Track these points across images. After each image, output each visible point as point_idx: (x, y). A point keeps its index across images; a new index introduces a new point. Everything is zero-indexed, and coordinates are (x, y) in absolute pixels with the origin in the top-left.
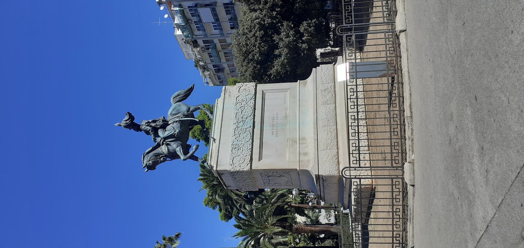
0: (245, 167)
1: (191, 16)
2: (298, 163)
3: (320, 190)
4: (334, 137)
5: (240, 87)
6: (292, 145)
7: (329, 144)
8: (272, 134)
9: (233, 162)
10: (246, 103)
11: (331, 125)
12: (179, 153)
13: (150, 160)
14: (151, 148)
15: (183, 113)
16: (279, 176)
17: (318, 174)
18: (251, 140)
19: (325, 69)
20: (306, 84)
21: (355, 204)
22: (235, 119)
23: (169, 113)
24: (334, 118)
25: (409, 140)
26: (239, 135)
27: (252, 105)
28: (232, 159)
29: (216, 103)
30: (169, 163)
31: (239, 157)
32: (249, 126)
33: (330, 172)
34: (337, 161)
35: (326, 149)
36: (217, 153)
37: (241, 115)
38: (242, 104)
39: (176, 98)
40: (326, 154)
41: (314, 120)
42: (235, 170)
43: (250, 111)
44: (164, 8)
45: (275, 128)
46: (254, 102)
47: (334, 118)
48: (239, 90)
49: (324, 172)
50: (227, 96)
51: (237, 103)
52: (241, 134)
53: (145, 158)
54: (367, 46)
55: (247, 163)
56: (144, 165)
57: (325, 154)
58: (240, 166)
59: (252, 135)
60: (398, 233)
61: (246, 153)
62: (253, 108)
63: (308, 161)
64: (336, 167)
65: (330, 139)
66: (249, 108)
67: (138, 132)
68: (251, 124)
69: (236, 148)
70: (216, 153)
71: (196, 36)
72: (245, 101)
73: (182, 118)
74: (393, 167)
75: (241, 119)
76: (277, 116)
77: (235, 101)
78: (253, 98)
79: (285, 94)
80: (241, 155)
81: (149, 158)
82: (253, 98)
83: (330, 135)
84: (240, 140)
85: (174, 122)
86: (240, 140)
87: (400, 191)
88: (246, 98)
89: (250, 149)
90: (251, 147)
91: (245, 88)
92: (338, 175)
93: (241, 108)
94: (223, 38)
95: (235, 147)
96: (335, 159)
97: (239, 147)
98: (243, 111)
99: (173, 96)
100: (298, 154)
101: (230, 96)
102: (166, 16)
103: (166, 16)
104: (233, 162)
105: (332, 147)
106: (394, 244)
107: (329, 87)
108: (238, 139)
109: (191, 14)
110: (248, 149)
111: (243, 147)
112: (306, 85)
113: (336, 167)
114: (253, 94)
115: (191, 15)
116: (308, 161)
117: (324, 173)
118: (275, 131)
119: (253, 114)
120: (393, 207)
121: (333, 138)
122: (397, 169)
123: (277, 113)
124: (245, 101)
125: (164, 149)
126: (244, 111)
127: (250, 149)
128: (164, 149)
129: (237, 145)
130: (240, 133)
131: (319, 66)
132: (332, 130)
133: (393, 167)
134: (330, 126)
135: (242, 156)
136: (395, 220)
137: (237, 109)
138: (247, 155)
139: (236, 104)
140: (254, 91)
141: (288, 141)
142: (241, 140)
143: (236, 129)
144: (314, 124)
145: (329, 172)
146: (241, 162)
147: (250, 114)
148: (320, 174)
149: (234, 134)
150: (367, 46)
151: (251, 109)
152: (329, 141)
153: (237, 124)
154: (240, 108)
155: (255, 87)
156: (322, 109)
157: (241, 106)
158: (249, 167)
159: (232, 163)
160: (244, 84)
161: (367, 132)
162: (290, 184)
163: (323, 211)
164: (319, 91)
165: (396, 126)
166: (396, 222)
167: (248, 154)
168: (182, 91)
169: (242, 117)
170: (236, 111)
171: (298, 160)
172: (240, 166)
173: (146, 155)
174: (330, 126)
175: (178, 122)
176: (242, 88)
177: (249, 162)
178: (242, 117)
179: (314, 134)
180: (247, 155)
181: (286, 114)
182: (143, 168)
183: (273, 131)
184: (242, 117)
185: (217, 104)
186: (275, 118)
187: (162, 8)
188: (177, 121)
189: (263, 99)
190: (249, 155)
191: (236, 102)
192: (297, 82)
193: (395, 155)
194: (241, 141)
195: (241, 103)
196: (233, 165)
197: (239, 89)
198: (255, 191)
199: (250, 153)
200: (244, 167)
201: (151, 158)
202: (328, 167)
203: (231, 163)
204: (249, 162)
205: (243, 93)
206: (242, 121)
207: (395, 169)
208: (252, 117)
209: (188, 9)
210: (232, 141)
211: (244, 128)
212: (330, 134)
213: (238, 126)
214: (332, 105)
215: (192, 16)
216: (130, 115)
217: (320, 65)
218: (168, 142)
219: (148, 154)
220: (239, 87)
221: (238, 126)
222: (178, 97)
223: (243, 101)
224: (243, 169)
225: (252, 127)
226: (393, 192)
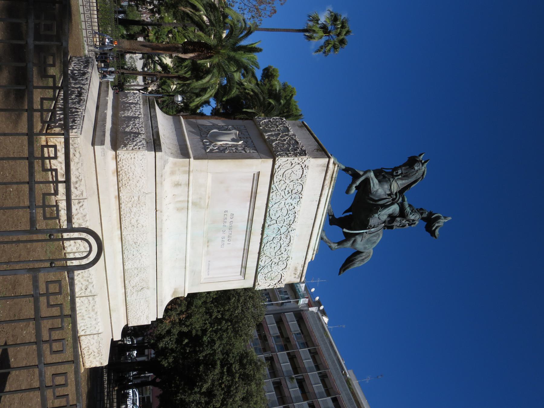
0: (284, 163)
2: (191, 169)
4: (126, 217)
5: (279, 282)
6: (200, 198)
7: (134, 205)
8: (233, 214)
9: (303, 171)
10: (272, 261)
11: (131, 235)
12: (376, 181)
13: (417, 171)
14: (412, 187)
15: (363, 238)
17: (156, 153)
18: (270, 205)
19: (142, 320)
20: (175, 292)
21: (57, 130)
22: (292, 237)
23: (381, 237)
24: (125, 247)
26: (288, 213)
27: (263, 258)
28: (303, 176)
29: (314, 255)
30: (388, 165)
31: (291, 180)
32: (271, 227)
33: (133, 157)
34: (121, 176)
36: (325, 184)
37: (282, 243)
38: (278, 259)
39: (366, 256)
40: (140, 188)
42: (300, 158)
43: (268, 250)
44: (315, 298)
45: (228, 224)
46: (260, 263)
47: (125, 247)
48: (281, 279)
49: (144, 157)
51: (286, 260)
52: (285, 215)
53: (422, 173)
54: (86, 252)
55: (279, 169)
56: (425, 165)
58: (292, 164)
59: (268, 214)
61: (280, 186)
62: (263, 254)
63: (173, 173)
64: (121, 165)
65: (133, 213)
66: (268, 254)
67: (166, 63)
68: (268, 230)
69: (296, 193)
70: (326, 185)
72: (273, 263)
73: (366, 232)
75: (282, 237)
76: (223, 243)
78: (260, 269)
79: (208, 275)
80: (288, 181)
81: (417, 174)
82: (260, 269)
83: (132, 220)
84: (287, 206)
85: (377, 227)
86: (288, 205)
88: (272, 268)
89: (273, 191)
90: (271, 195)
91: (271, 281)
92: (117, 152)
93: (280, 253)
96: (123, 180)
97: (290, 194)
98: (278, 249)
99: (370, 257)
100: (191, 184)
101: (296, 269)
102: (313, 290)
103: (313, 290)
104: (303, 171)
105: (130, 200)
107: (135, 294)
108: (291, 207)
110: (277, 191)
111: (284, 195)
112: (174, 290)
114: (260, 274)
115: (288, 293)
116: (173, 173)
117: (144, 155)
118: (229, 220)
119: (263, 245)
121: (128, 215)
123: (222, 246)
124: (273, 263)
125: (396, 186)
126: (276, 249)
127: (273, 191)
128: (396, 186)
129: (293, 198)
130: (287, 216)
131: (151, 321)
132: (130, 228)
134: (133, 234)
135: (286, 181)
137: (287, 251)
138: (279, 183)
139: (287, 259)
140: (259, 278)
141: (208, 205)
142: (286, 205)
143: (292, 221)
144: (161, 236)
145: (136, 156)
146: (290, 171)
147: (267, 244)
148: (153, 153)
149: (296, 214)
150: (86, 252)
151: (265, 252)
152: (134, 210)
153: (290, 229)
154: (282, 253)
155: (257, 284)
156: (148, 260)
157: (280, 256)
158: (277, 162)
159: (304, 169)
160: (273, 286)
163: (139, 69)
164: (153, 285)
167: (276, 184)
168: (358, 264)
169: (280, 240)
170: (289, 248)
171: (191, 174)
172: (292, 164)
173: (420, 178)
174: (133, 234)
175: (372, 227)
176: (276, 281)
177: (277, 170)
178: (280, 240)
179: (162, 220)
180: (278, 183)
181: (208, 246)
182: (428, 160)
183: (231, 220)
184: (281, 240)
185: (313, 254)
186: (226, 240)
187: (317, 298)
188: (373, 228)
189: (244, 267)
190: (275, 182)
191: (287, 262)
192: (188, 294)
194: (286, 203)
195: (280, 259)
196: (303, 167)
197: (282, 280)
199: (273, 186)
200: (286, 162)
201: (414, 173)
202: (136, 165)
203: (306, 169)
204: (276, 171)
205: (275, 275)
206: (281, 234)
208: (265, 241)
210: (300, 203)
211: (279, 224)
212: (134, 221)
213: (289, 226)
214: (130, 267)
216: (433, 234)
218: (389, 197)
219: (417, 180)
220: (280, 282)
221: (289, 226)
222: (364, 257)
223: (277, 264)
224: (288, 160)
225: (266, 225)
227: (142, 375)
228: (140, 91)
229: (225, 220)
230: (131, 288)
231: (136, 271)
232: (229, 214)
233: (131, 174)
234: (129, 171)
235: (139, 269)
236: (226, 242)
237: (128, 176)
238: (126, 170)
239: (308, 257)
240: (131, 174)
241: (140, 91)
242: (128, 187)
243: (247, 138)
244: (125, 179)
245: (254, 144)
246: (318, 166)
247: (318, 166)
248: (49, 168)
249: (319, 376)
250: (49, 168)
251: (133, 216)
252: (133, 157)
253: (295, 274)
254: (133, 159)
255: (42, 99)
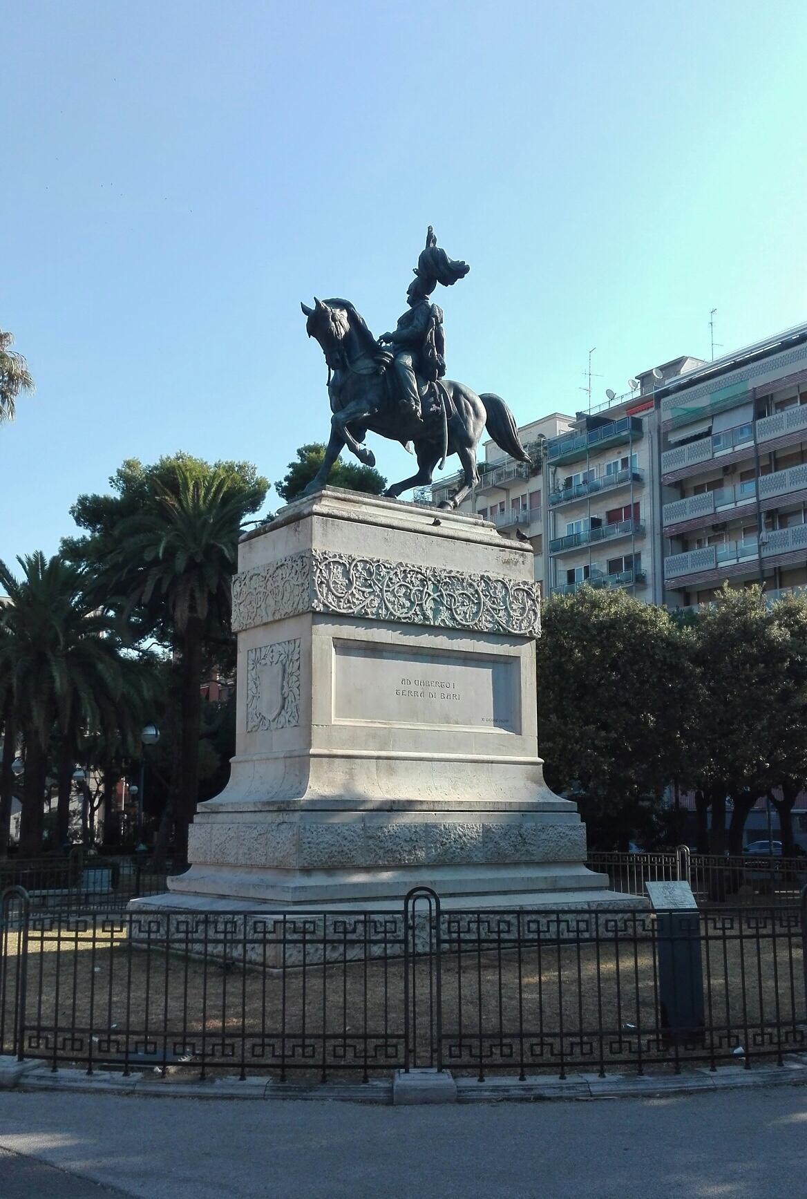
1: (609, 463)
3: (448, 811)
8: (403, 680)
16: (286, 695)
25: (523, 1089)
33: (308, 845)
34: (336, 864)
35: (368, 834)
41: (427, 802)
49: (308, 827)
50: (507, 554)
57: (355, 832)
60: (160, 1049)
65: (395, 848)
71: (554, 473)
74: (440, 1041)
77: (493, 576)
87: (286, 1060)
94: (543, 548)
95: (372, 572)
101: (507, 562)
106: (558, 1040)
107: (530, 848)
109: (616, 463)
113: (319, 864)
118: (413, 687)
120: (318, 1037)
122: (433, 1051)
123: (457, 697)
133: (440, 1041)
136: (475, 1042)
143: (419, 576)
161: (345, 961)
162: (251, 725)
165: (476, 1051)
166: (551, 1045)
183: (413, 683)
186: (446, 691)
193: (360, 1047)
198: (232, 621)
202: (320, 840)
207: (435, 1046)
209: (446, 458)
215: (608, 466)
217: (584, 824)
226: (562, 1035)
227: (14, 830)
228: (95, 806)
229: (407, 693)
230: (518, 855)
231: (490, 845)
232: (403, 687)
233: (334, 848)
234: (329, 851)
235: (487, 840)
236: (450, 691)
237: (336, 854)
238: (326, 856)
239: (486, 539)
240: (334, 848)
241: (95, 806)
242: (353, 853)
243: (272, 652)
244: (340, 857)
245: (284, 642)
246: (325, 534)
247: (325, 534)
248: (302, 968)
249: (776, 470)
250: (302, 968)
251: (399, 848)
252: (308, 845)
253: (516, 563)
254: (311, 845)
255: (193, 1045)
